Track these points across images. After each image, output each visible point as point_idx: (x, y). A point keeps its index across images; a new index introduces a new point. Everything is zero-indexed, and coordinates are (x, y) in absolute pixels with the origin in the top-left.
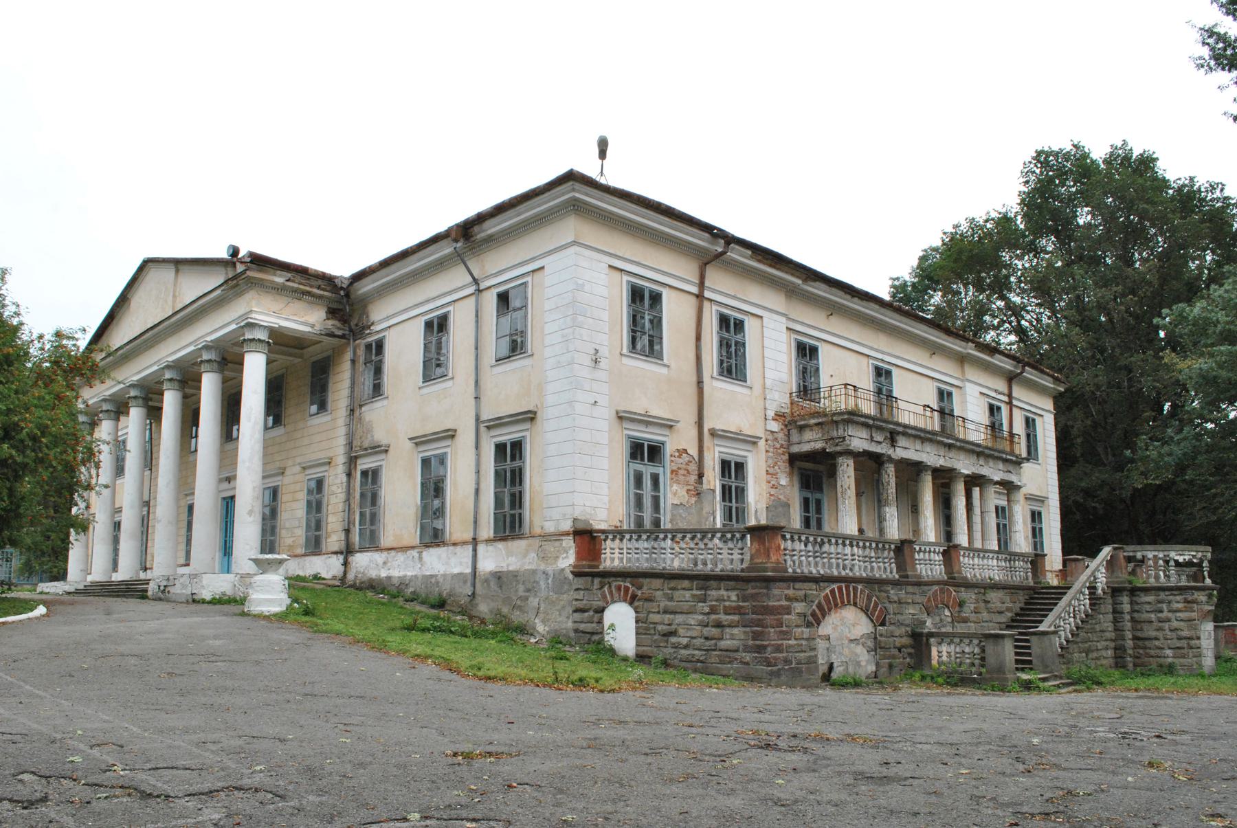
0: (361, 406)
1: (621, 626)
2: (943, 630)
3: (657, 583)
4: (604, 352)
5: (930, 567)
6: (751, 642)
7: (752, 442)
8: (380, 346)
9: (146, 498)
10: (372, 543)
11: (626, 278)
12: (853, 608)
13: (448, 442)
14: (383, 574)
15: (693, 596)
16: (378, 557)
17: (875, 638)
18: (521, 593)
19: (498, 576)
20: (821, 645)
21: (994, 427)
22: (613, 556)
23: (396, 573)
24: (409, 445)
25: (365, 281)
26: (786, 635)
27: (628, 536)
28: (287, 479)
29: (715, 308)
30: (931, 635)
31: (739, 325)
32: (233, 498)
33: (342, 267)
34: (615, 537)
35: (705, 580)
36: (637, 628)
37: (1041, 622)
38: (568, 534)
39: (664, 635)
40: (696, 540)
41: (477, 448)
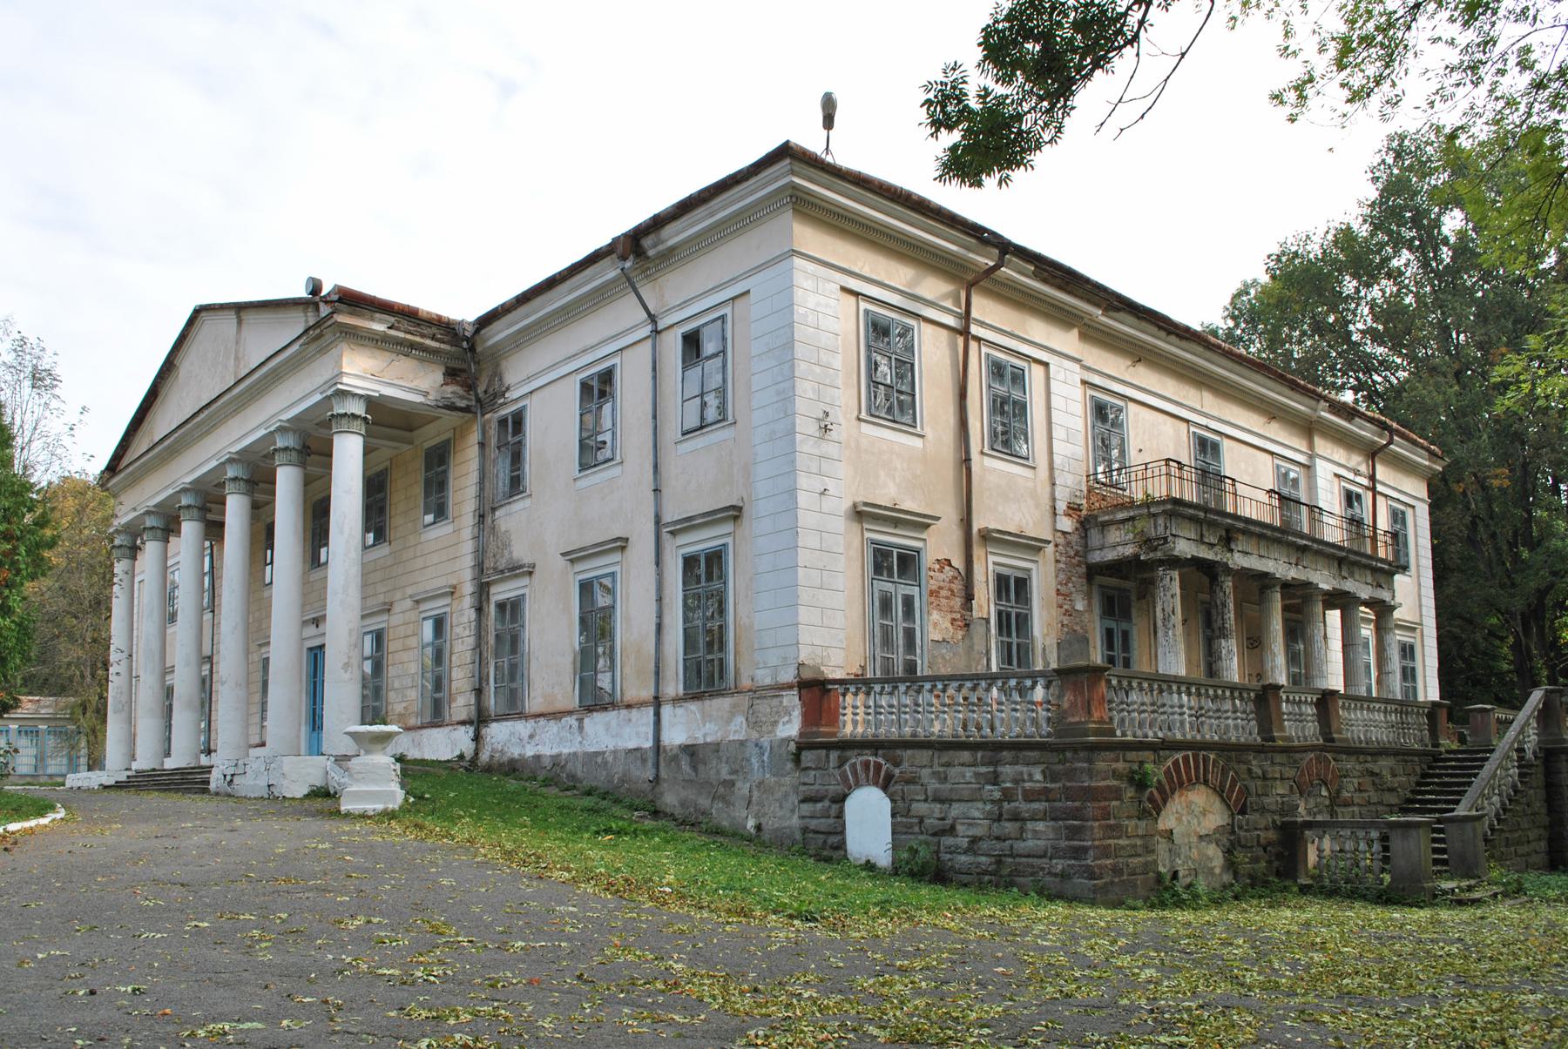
0: (494, 510)
1: (869, 821)
2: (1319, 818)
3: (923, 756)
4: (837, 415)
5: (1298, 725)
6: (1064, 844)
7: (1032, 546)
8: (518, 421)
9: (207, 651)
10: (514, 710)
11: (863, 305)
12: (1202, 788)
13: (616, 557)
14: (530, 752)
15: (977, 775)
16: (522, 728)
17: (1233, 832)
18: (725, 775)
19: (690, 750)
20: (1162, 846)
21: (1355, 522)
22: (854, 718)
23: (547, 750)
24: (561, 562)
25: (496, 326)
26: (1116, 830)
27: (877, 688)
28: (396, 619)
29: (984, 350)
30: (1309, 825)
31: (1018, 378)
32: (322, 647)
33: (464, 309)
34: (858, 689)
35: (993, 750)
36: (893, 825)
37: (1457, 802)
38: (790, 687)
39: (935, 834)
40: (964, 691)
41: (657, 564)
